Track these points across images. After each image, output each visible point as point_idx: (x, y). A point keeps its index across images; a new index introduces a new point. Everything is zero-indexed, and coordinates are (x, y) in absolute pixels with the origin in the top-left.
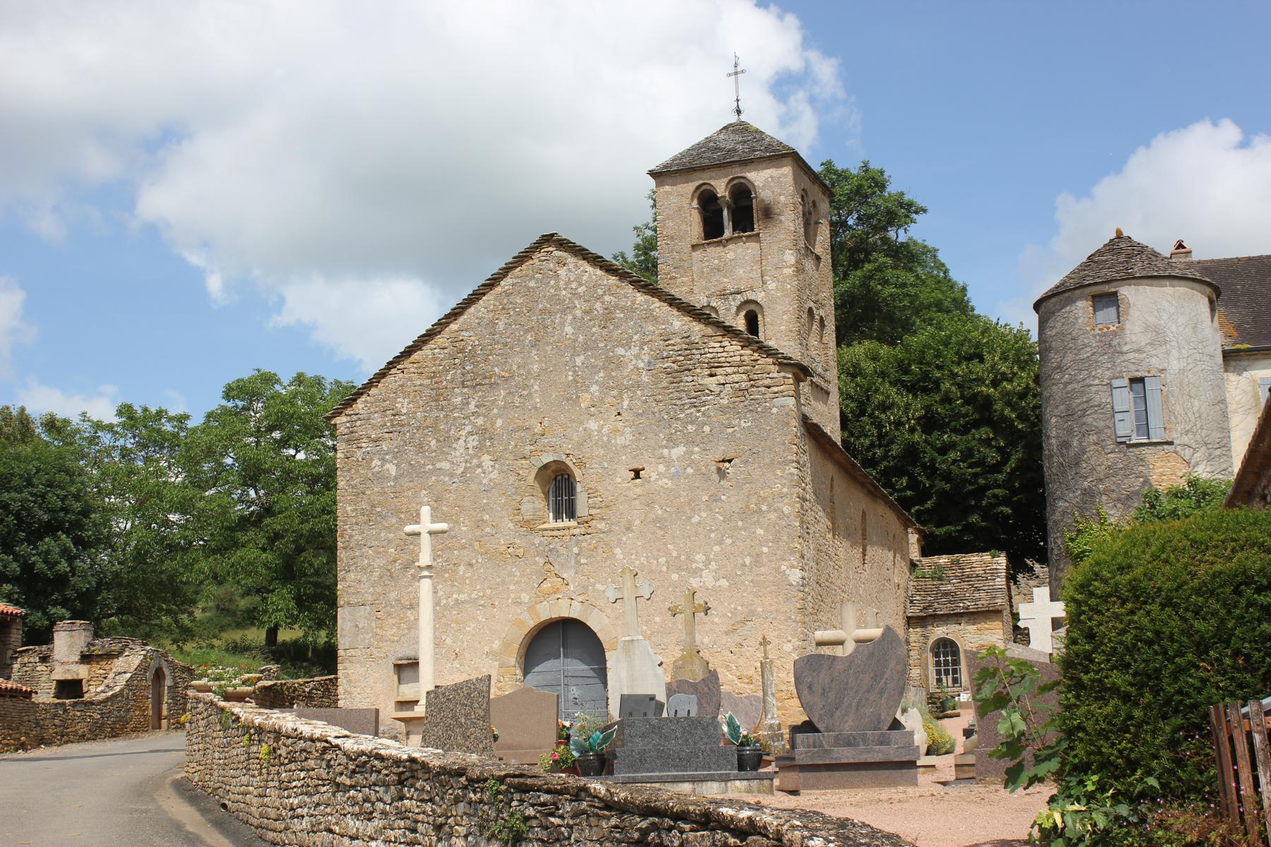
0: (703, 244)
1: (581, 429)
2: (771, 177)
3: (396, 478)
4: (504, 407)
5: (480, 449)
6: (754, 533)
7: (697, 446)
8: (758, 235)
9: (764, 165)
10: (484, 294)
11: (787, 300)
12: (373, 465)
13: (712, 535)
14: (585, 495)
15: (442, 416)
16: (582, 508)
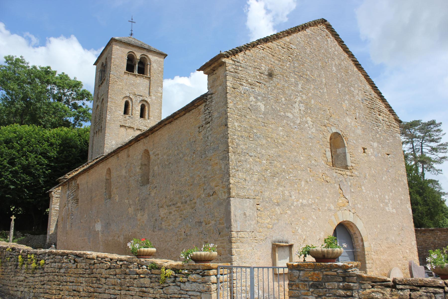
3: (264, 114)
9: (155, 55)
11: (158, 105)
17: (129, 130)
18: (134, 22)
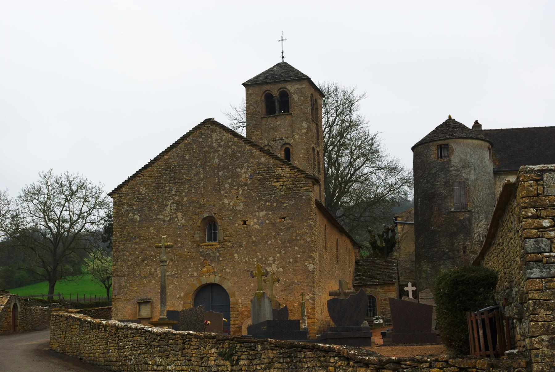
0: (266, 117)
1: (221, 203)
2: (297, 88)
4: (187, 192)
5: (177, 210)
6: (294, 249)
7: (271, 211)
8: (291, 114)
10: (180, 143)
11: (303, 143)
12: (129, 215)
13: (276, 249)
14: (222, 231)
15: (160, 195)
16: (220, 237)
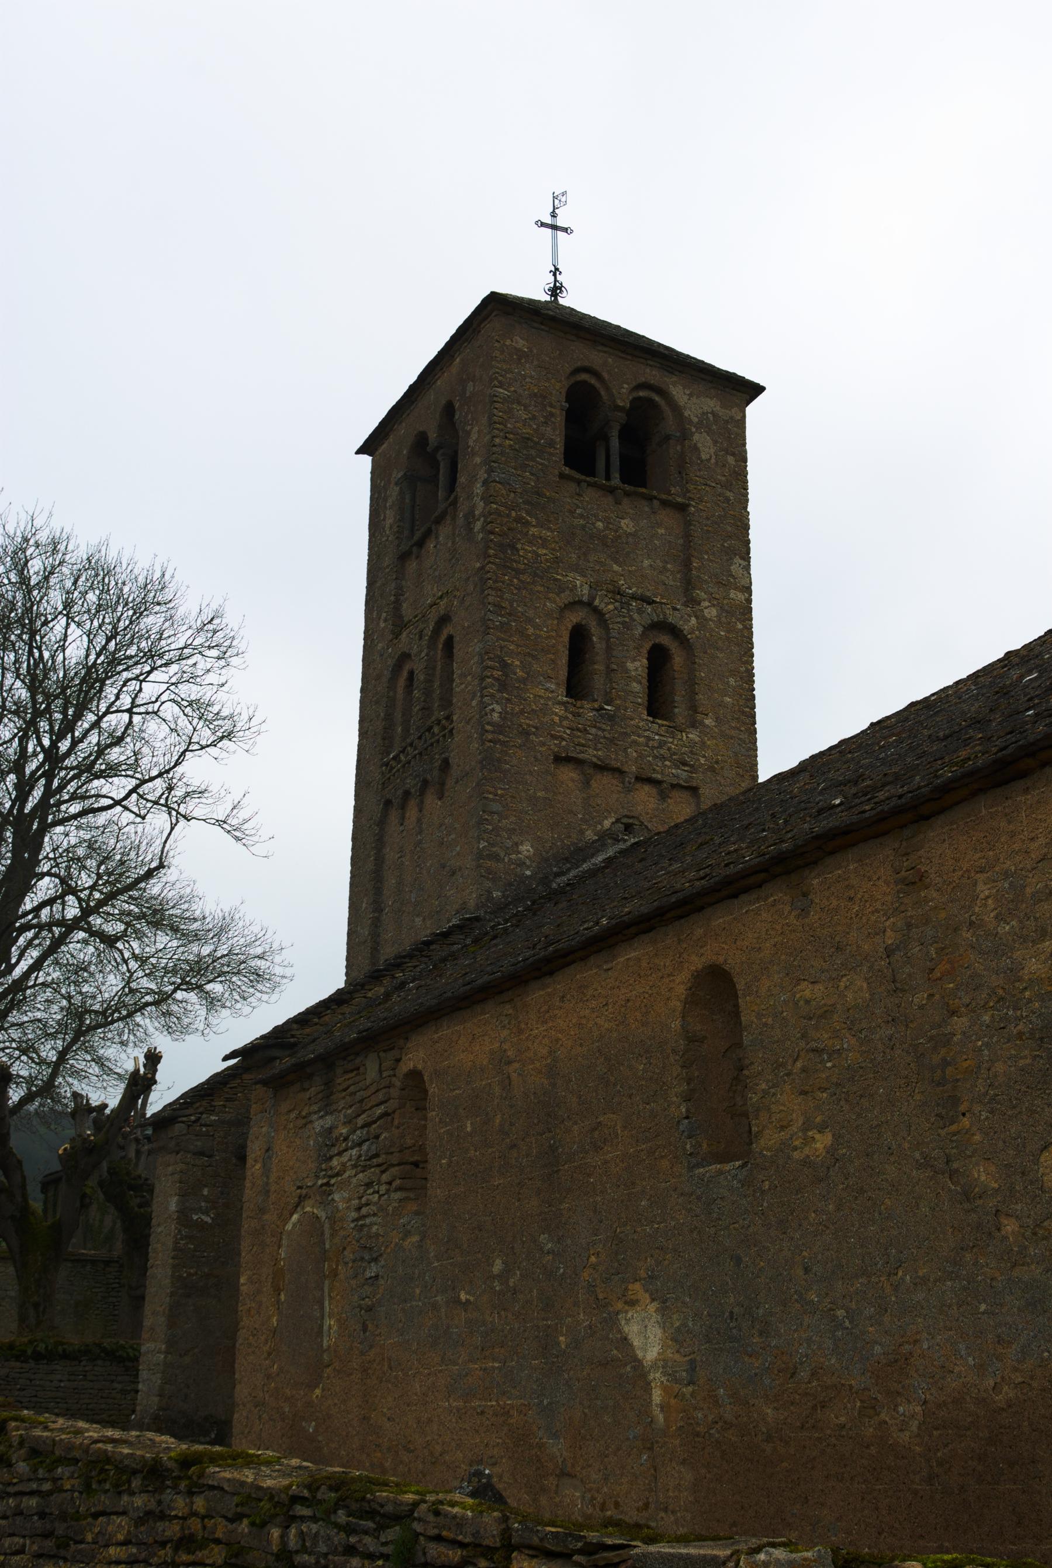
17: (603, 782)
18: (565, 230)
